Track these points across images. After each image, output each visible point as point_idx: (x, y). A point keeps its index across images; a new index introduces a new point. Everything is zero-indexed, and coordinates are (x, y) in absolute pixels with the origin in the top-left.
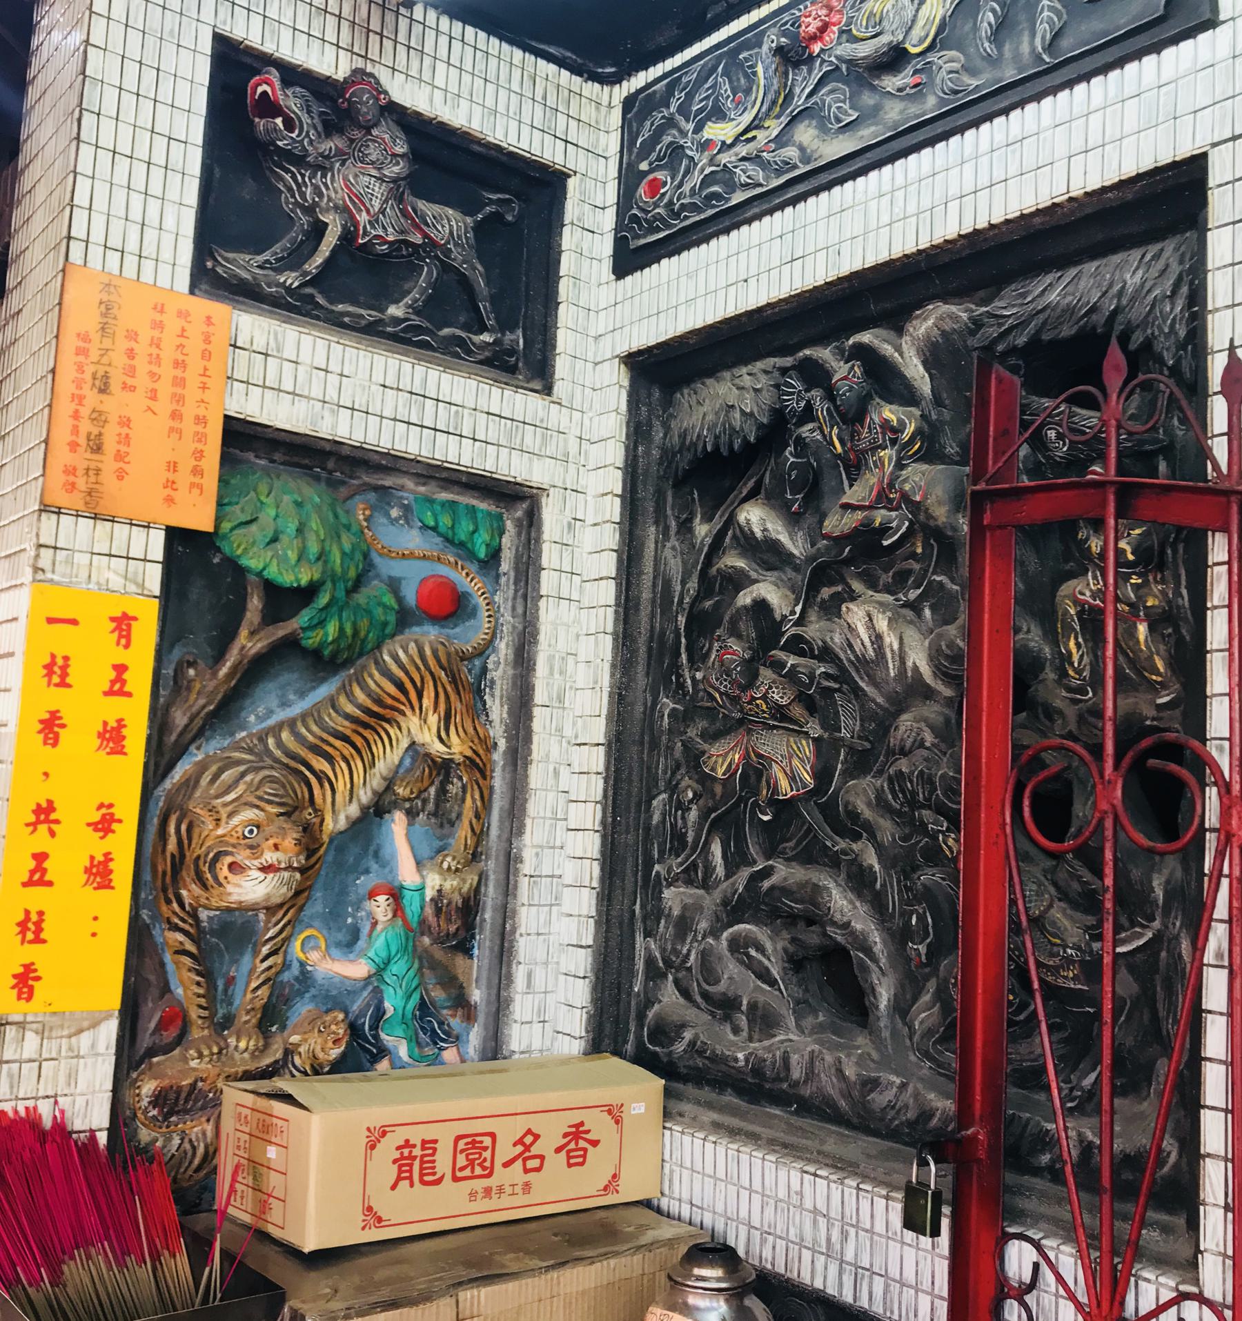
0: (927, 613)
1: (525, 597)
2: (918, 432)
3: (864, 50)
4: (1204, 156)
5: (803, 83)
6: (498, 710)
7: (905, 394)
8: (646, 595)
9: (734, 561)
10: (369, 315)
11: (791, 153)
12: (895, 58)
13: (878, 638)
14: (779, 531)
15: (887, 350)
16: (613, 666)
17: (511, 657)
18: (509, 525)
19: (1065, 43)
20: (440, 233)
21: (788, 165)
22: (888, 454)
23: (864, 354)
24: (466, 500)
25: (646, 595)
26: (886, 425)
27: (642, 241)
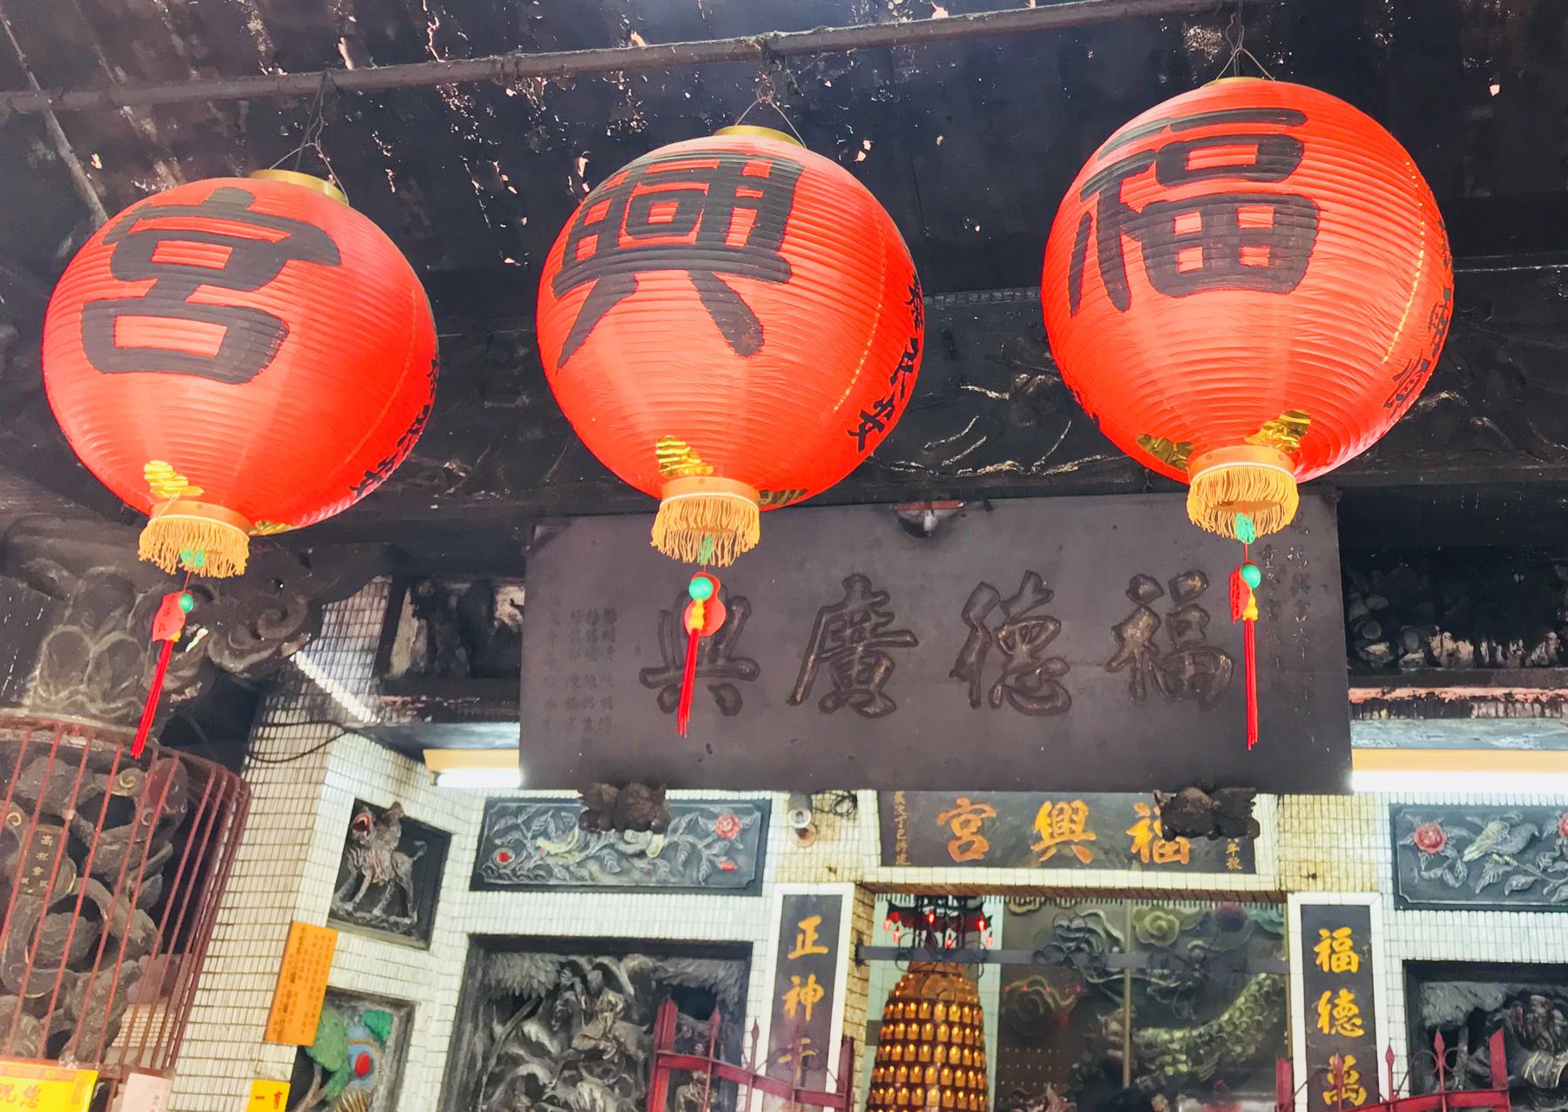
3: (630, 849)
7: (619, 989)
8: (461, 1062)
10: (368, 916)
11: (584, 873)
13: (594, 1101)
14: (544, 1039)
15: (614, 968)
21: (582, 878)
23: (601, 967)
25: (461, 1062)
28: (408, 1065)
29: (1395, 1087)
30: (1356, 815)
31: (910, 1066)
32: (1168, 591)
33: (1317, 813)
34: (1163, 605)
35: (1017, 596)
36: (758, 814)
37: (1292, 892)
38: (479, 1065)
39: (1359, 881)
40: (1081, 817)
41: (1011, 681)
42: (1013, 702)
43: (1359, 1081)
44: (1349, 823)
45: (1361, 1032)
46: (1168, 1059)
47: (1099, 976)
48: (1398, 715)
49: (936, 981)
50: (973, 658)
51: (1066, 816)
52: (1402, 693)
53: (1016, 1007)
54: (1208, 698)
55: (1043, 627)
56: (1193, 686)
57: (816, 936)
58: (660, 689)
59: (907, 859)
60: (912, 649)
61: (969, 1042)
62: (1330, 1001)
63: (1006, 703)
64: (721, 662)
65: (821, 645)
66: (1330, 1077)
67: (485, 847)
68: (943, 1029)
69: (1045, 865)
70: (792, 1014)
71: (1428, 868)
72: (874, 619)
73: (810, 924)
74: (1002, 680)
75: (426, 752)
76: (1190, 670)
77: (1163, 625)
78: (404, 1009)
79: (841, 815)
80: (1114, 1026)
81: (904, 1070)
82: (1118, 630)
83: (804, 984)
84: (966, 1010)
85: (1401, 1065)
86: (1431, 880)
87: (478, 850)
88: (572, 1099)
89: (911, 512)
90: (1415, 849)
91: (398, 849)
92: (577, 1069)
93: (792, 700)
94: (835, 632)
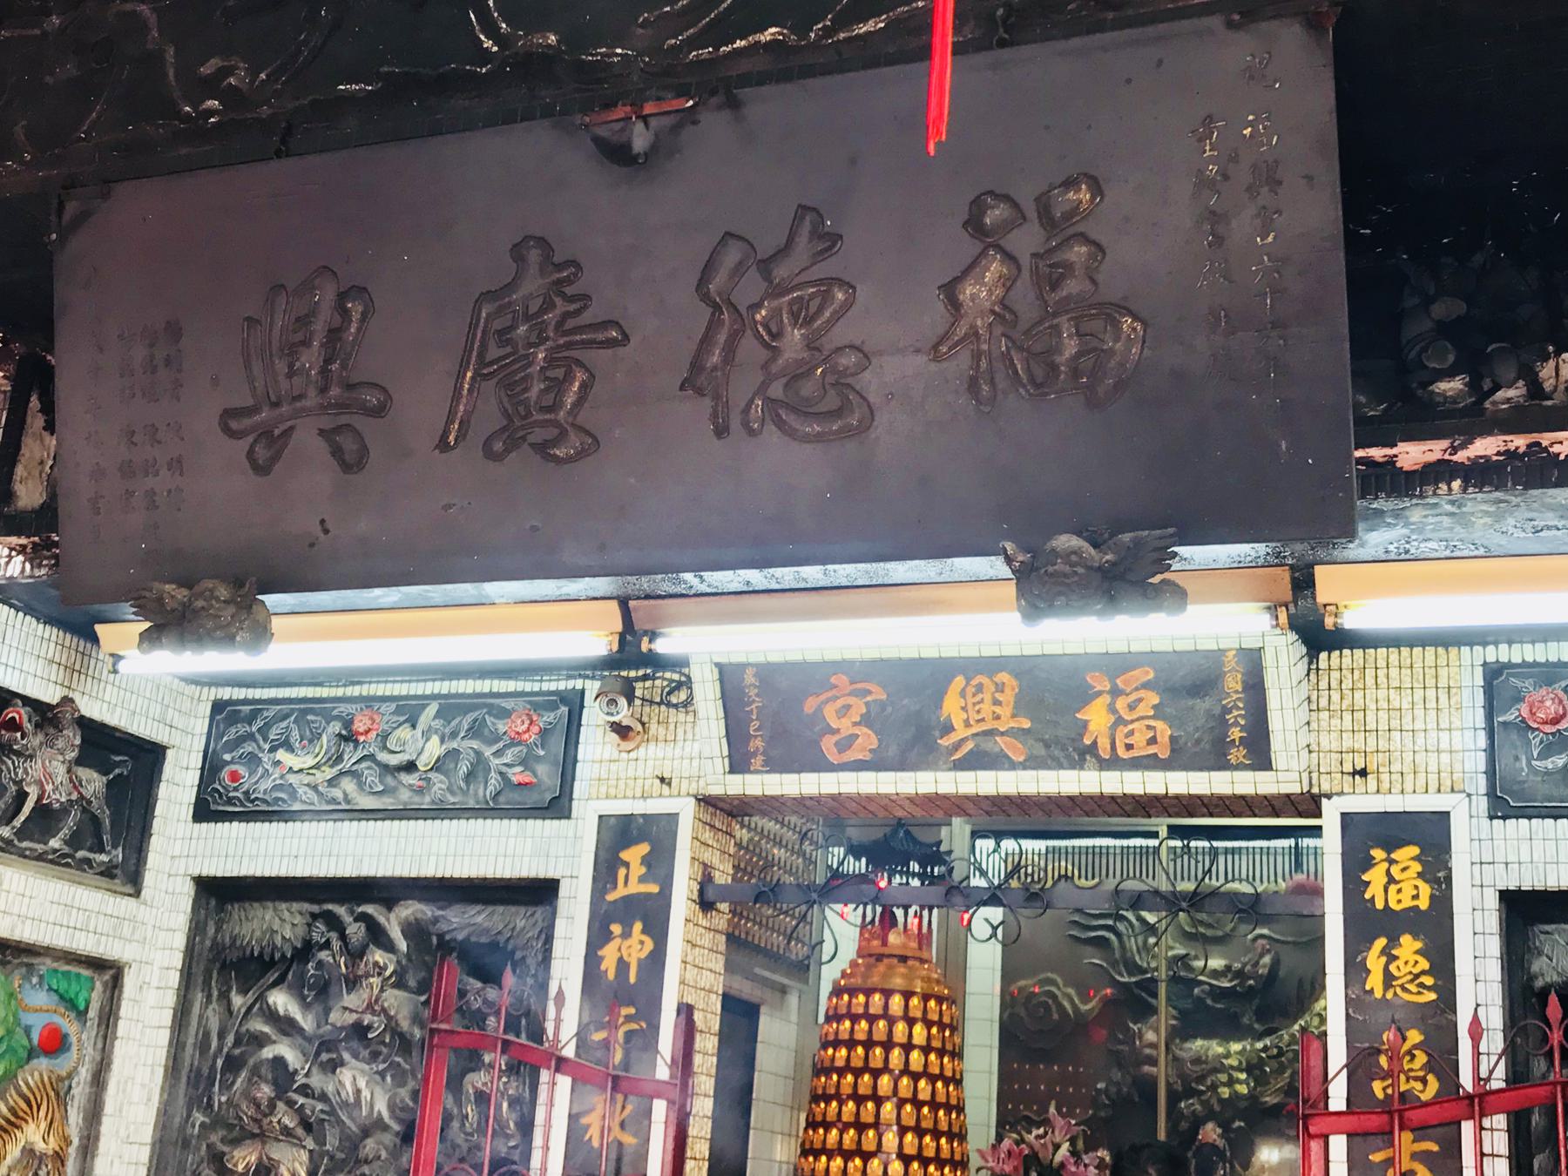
0: (389, 1079)
1: (105, 1038)
2: (394, 972)
3: (394, 760)
4: (558, 881)
5: (350, 757)
6: (75, 1118)
7: (390, 947)
8: (191, 1041)
9: (260, 1026)
10: (40, 847)
11: (337, 793)
12: (410, 767)
13: (358, 1091)
15: (382, 920)
16: (162, 1088)
17: (89, 1078)
18: (98, 985)
19: (502, 799)
20: (88, 791)
21: (334, 801)
22: (375, 981)
24: (74, 969)
25: (191, 1041)
26: (376, 964)
27: (221, 808)
28: (117, 1043)
29: (1484, 1073)
30: (1430, 682)
31: (858, 1073)
32: (1031, 213)
33: (1370, 681)
34: (1027, 240)
35: (784, 251)
36: (564, 709)
37: (1329, 796)
38: (214, 1044)
39: (1433, 778)
40: (1008, 697)
41: (776, 390)
42: (780, 424)
43: (1429, 1067)
44: (1419, 694)
45: (1432, 996)
46: (1223, 1077)
47: (1130, 974)
48: (1480, 486)
49: (890, 967)
50: (715, 358)
51: (988, 697)
52: (1486, 447)
53: (1023, 1013)
54: (1101, 390)
55: (826, 297)
56: (1075, 373)
57: (643, 870)
58: (250, 439)
59: (766, 763)
60: (621, 351)
61: (936, 1044)
62: (1384, 952)
63: (771, 428)
64: (335, 391)
65: (481, 355)
66: (1383, 1061)
67: (211, 768)
68: (901, 1027)
69: (960, 766)
70: (611, 975)
71: (1541, 757)
72: (561, 306)
73: (634, 855)
74: (762, 390)
75: (98, 628)
76: (1070, 347)
77: (1026, 274)
78: (110, 972)
79: (676, 706)
80: (1150, 1036)
81: (850, 1078)
82: (950, 292)
83: (626, 935)
84: (932, 1003)
85: (1494, 1042)
86: (1547, 773)
87: (203, 769)
88: (330, 1089)
89: (608, 123)
90: (1524, 727)
91: (79, 762)
92: (337, 1051)
93: (443, 445)
94: (500, 333)
